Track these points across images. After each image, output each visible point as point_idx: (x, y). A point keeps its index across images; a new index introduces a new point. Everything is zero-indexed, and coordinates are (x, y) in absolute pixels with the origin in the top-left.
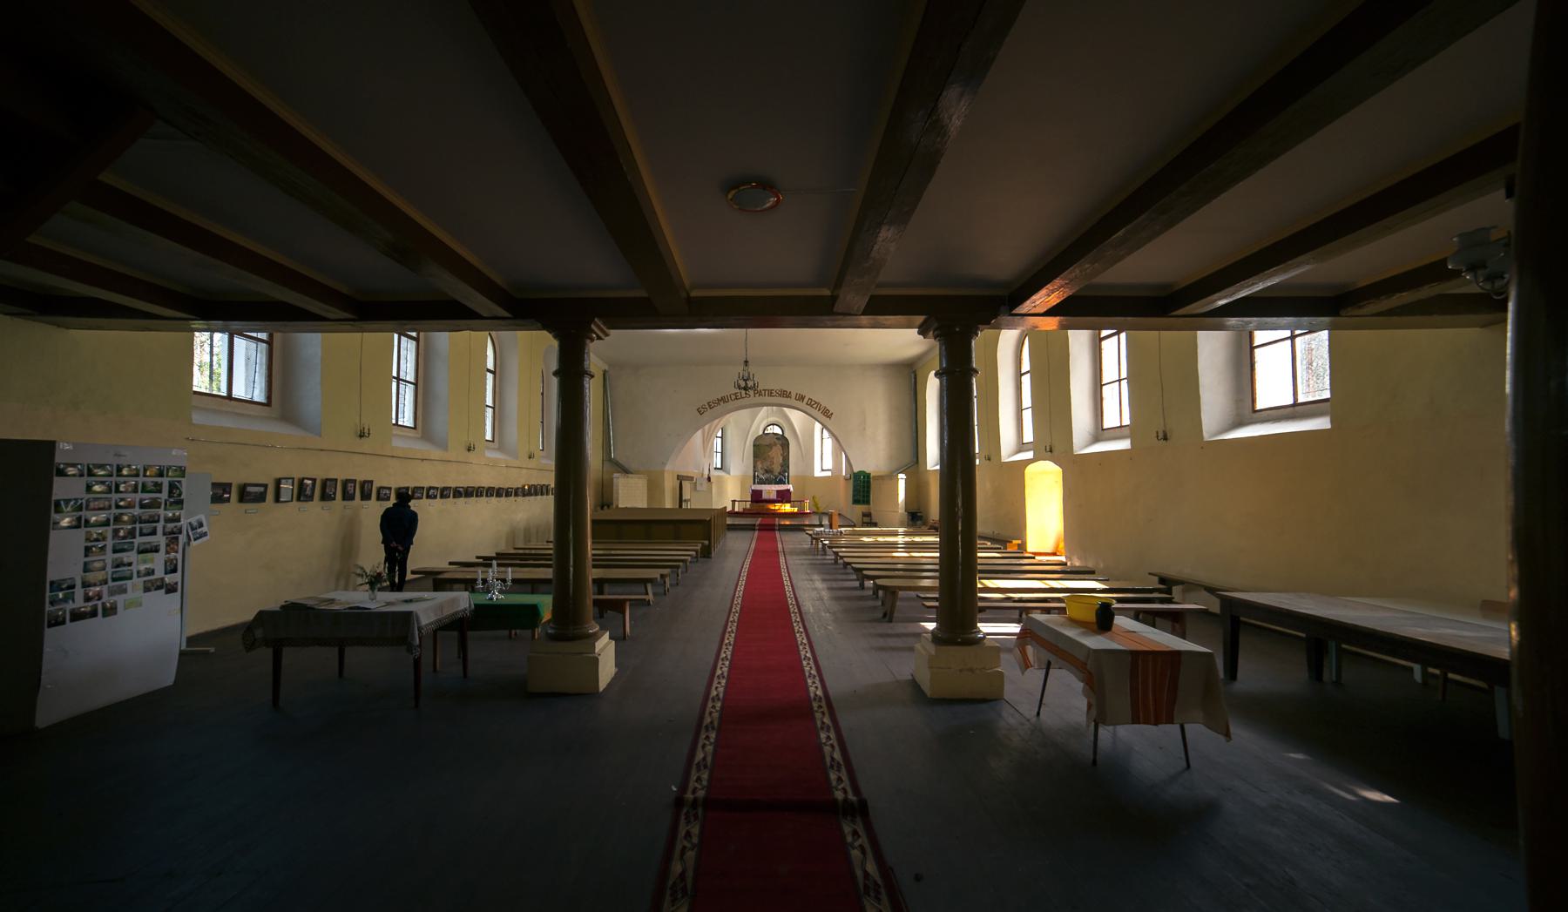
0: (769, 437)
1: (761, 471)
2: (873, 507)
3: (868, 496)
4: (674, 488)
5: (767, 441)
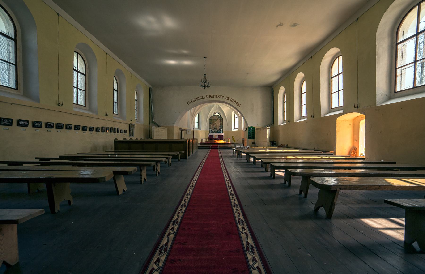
0: (215, 116)
1: (212, 129)
2: (255, 140)
3: (254, 136)
4: (178, 133)
5: (215, 118)
